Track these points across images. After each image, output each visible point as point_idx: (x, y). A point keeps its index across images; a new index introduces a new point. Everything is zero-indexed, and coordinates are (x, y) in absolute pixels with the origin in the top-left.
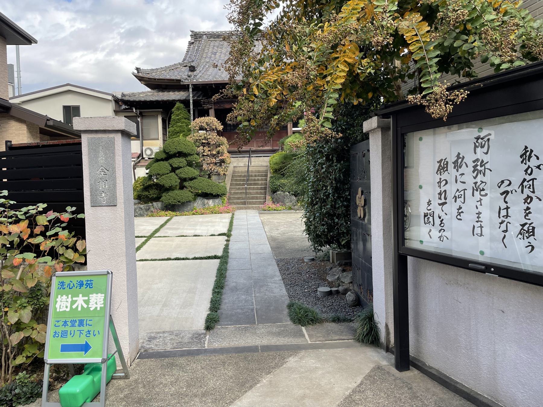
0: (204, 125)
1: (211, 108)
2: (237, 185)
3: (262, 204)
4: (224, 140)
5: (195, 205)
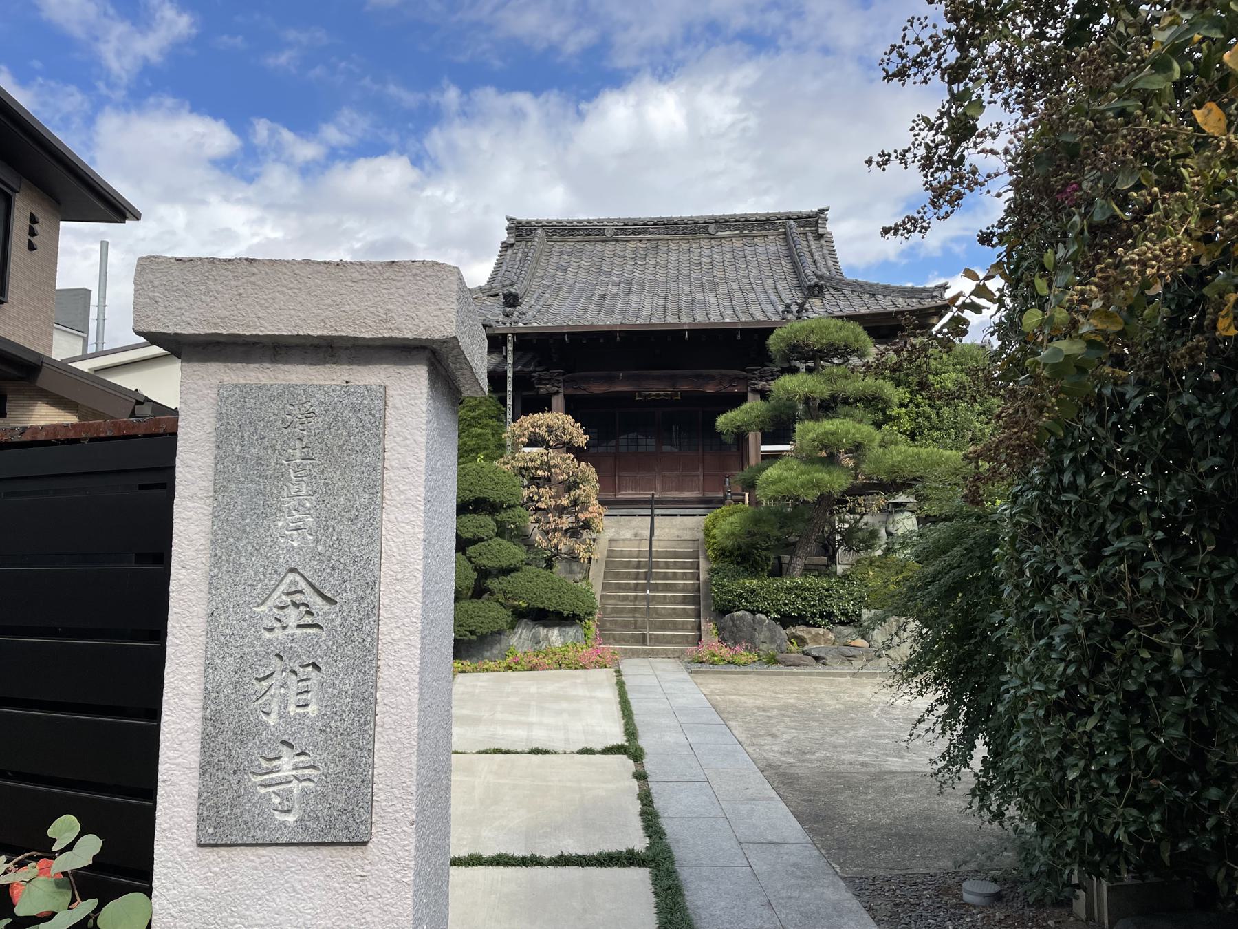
0: (542, 431)
1: (558, 393)
2: (620, 587)
3: (689, 644)
4: (589, 470)
5: (514, 641)
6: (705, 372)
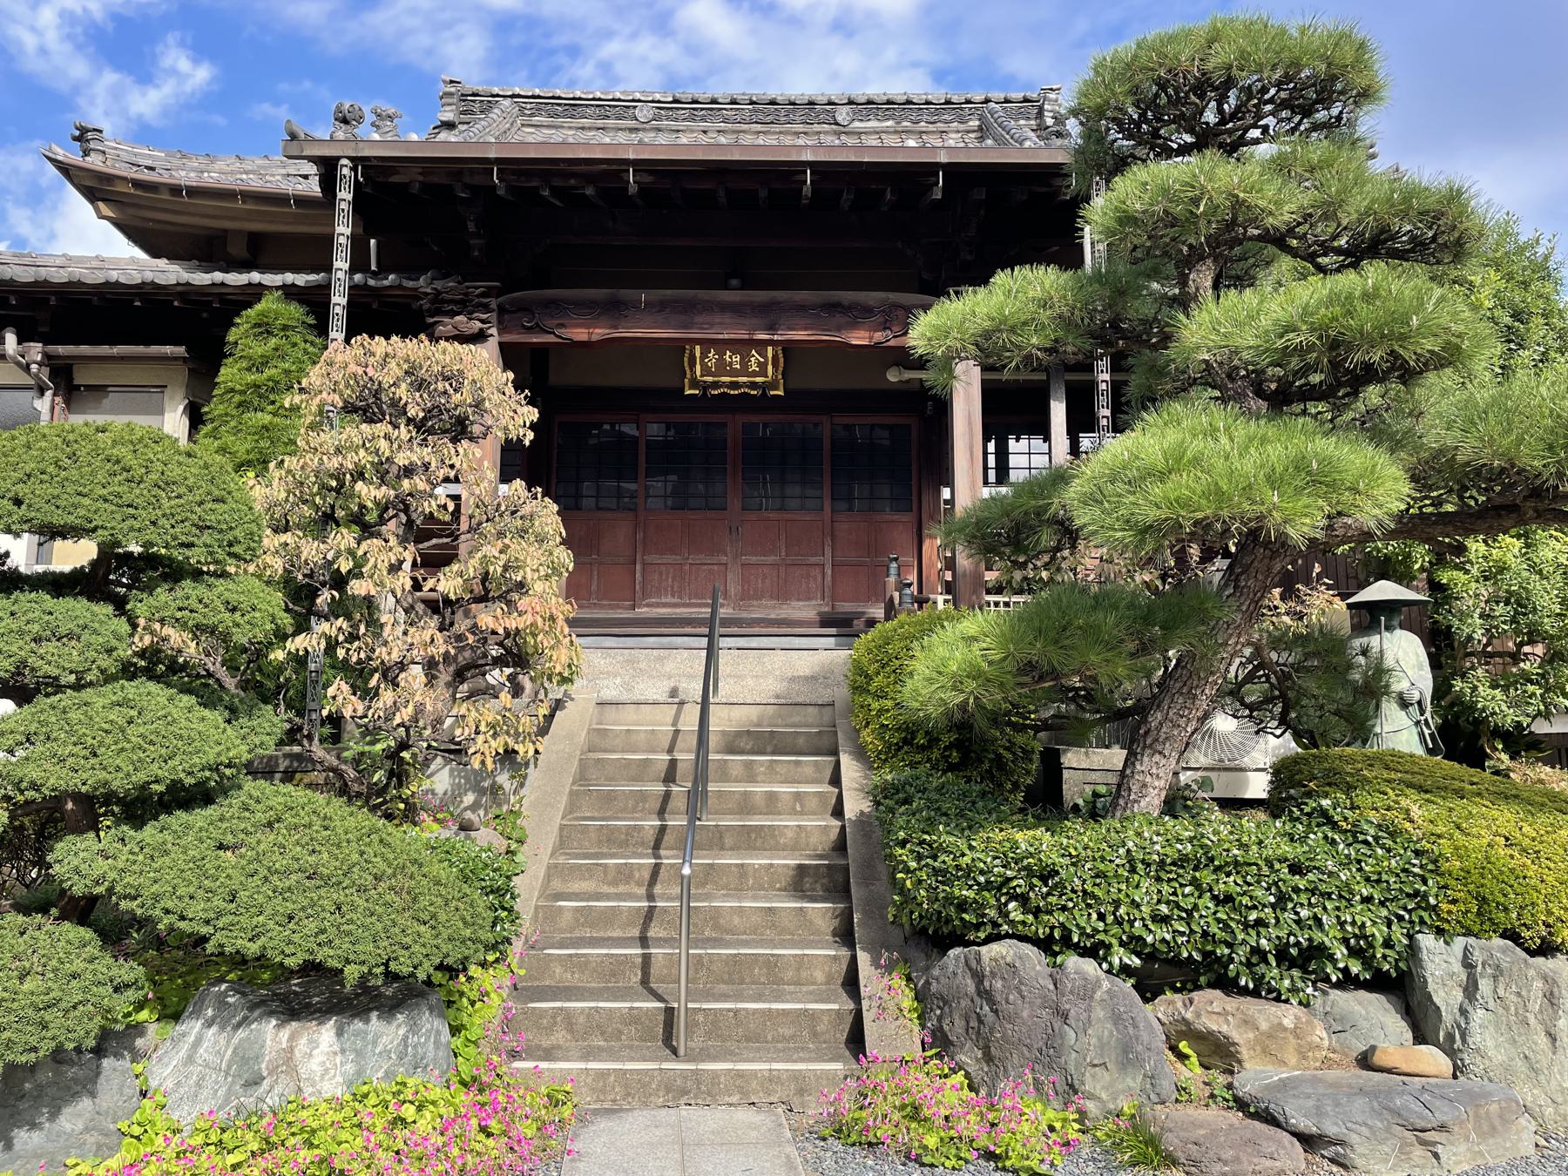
6: (847, 296)
